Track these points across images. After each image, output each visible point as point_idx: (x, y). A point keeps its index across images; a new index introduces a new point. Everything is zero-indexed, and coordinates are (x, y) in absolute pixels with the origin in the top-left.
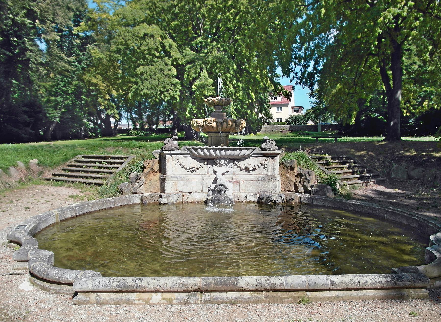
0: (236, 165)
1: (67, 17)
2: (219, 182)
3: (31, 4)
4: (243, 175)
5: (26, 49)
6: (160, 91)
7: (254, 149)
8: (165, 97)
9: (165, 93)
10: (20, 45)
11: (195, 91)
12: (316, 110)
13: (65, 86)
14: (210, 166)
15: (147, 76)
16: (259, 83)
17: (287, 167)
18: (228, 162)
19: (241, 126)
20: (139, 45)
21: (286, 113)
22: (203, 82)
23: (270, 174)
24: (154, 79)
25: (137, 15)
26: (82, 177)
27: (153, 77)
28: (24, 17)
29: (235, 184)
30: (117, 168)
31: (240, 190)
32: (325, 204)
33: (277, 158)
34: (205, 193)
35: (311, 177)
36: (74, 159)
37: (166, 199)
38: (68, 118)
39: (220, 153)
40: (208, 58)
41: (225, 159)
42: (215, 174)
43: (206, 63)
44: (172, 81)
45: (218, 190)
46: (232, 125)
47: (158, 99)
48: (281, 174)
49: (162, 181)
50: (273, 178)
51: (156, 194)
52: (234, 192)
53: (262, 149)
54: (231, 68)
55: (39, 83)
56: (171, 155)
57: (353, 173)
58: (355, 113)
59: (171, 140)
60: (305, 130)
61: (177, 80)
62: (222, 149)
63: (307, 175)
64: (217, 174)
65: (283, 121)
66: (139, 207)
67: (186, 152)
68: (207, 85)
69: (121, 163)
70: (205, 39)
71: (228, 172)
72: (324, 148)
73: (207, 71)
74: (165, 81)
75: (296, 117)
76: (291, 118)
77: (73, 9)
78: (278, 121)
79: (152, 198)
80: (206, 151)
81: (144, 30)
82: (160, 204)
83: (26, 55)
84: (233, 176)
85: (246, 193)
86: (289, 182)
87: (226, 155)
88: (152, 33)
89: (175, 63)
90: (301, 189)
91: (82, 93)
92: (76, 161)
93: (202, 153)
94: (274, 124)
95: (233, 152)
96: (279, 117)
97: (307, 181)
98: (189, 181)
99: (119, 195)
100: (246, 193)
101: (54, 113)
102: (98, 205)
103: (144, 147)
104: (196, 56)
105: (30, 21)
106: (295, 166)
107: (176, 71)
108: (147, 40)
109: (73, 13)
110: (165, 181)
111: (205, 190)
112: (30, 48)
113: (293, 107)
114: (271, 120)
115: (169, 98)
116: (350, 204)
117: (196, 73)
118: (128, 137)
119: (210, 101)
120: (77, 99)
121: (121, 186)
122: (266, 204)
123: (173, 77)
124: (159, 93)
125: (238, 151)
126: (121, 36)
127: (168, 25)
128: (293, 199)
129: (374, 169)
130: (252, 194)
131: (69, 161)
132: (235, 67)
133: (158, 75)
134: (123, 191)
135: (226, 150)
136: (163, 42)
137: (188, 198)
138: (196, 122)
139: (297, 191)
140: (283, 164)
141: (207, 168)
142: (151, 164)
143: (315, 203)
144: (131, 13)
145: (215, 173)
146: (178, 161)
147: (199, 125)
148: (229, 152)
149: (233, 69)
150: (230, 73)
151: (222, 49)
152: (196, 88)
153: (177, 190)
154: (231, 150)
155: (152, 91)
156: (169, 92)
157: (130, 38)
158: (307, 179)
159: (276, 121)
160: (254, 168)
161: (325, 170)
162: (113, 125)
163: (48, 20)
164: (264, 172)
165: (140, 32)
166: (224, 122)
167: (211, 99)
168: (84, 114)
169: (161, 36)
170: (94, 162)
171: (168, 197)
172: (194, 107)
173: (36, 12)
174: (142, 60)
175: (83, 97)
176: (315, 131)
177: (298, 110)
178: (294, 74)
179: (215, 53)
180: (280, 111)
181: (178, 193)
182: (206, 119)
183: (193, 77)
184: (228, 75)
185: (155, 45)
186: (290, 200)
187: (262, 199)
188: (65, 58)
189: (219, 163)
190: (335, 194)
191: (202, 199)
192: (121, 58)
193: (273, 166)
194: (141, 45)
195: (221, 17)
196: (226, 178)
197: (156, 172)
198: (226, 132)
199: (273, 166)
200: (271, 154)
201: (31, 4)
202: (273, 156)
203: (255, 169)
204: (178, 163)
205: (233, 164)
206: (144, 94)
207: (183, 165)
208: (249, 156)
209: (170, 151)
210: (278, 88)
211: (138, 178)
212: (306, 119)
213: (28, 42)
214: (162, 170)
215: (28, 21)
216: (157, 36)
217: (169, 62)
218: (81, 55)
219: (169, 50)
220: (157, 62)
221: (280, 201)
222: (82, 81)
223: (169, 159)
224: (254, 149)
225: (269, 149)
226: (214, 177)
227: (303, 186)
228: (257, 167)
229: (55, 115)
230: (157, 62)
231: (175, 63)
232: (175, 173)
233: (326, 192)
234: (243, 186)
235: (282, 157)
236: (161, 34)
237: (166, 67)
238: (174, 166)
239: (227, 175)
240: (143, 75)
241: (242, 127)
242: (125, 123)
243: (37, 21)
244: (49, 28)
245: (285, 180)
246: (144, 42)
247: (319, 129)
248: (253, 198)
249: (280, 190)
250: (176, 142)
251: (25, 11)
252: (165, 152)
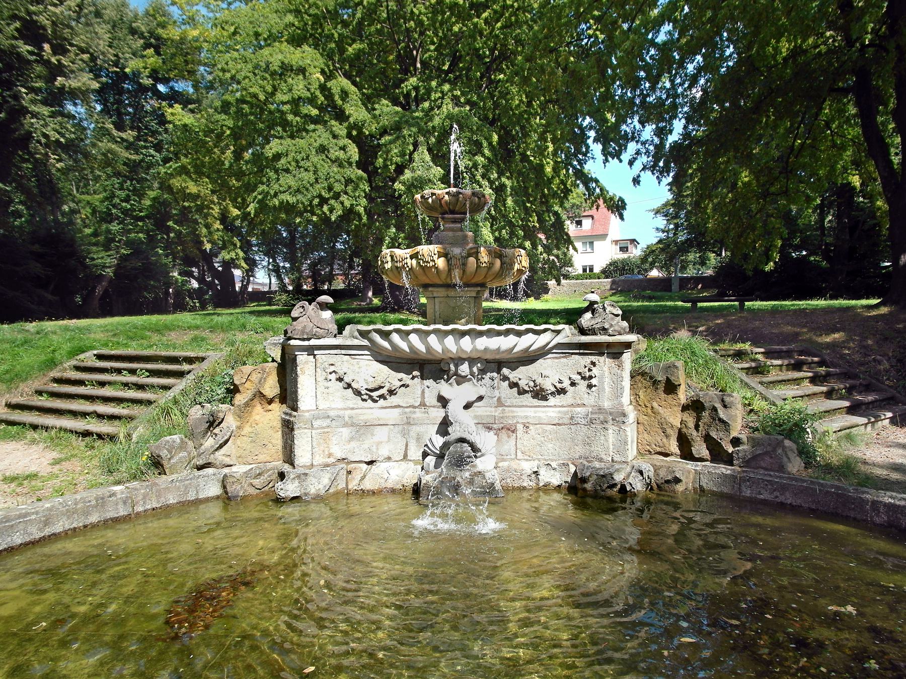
1: (130, 50)
2: (455, 432)
3: (33, 8)
5: (24, 111)
6: (320, 196)
7: (558, 332)
8: (331, 210)
9: (332, 202)
10: (8, 102)
11: (400, 196)
12: (669, 245)
13: (127, 200)
14: (430, 382)
15: (289, 163)
16: (550, 181)
17: (655, 383)
18: (483, 372)
19: (517, 267)
20: (269, 89)
21: (602, 255)
22: (419, 173)
23: (607, 404)
24: (306, 170)
25: (263, 25)
26: (74, 414)
27: (302, 163)
28: (16, 38)
30: (166, 388)
31: (519, 453)
32: (781, 499)
34: (416, 462)
35: (732, 411)
36: (74, 362)
37: (296, 483)
38: (136, 269)
39: (457, 343)
40: (431, 120)
42: (444, 407)
43: (427, 133)
44: (348, 173)
46: (491, 264)
47: (318, 215)
49: (288, 427)
51: (269, 466)
52: (501, 457)
53: (583, 331)
54: (485, 144)
55: (78, 195)
56: (311, 350)
57: (829, 395)
58: (779, 243)
59: (311, 308)
60: (644, 290)
61: (360, 172)
62: (463, 334)
63: (718, 406)
64: (450, 406)
65: (597, 270)
66: (215, 511)
67: (356, 342)
68: (430, 180)
69: (180, 374)
70: (423, 81)
71: (480, 398)
72: (729, 325)
73: (430, 150)
74: (331, 174)
75: (624, 262)
76: (613, 263)
77: (142, 33)
78: (584, 270)
79: (256, 482)
81: (280, 57)
82: (279, 501)
83: (22, 125)
84: (498, 412)
86: (663, 428)
88: (301, 63)
89: (354, 133)
90: (700, 449)
91: (169, 217)
92: (78, 368)
93: (404, 345)
94: (577, 278)
96: (588, 263)
97: (721, 426)
99: (152, 472)
100: (536, 462)
101: (102, 258)
102: (70, 513)
103: (267, 330)
104: (404, 116)
105: (29, 48)
106: (681, 378)
107: (357, 150)
108: (290, 80)
109: (142, 41)
110: (292, 430)
111: (415, 453)
112: (33, 108)
113: (616, 242)
114: (570, 269)
115: (340, 212)
116: (874, 503)
117: (402, 154)
118: (268, 308)
119: (430, 200)
120: (158, 229)
121: (157, 447)
122: (596, 495)
123: (350, 164)
124: (316, 201)
125: (512, 340)
126: (229, 71)
127: (342, 51)
128: (677, 481)
129: (878, 380)
130: (554, 464)
131: (58, 368)
132: (495, 138)
133: (315, 159)
134: (165, 463)
136: (329, 84)
138: (392, 257)
139: (687, 454)
140: (643, 374)
141: (420, 389)
142: (255, 377)
143: (747, 493)
144: (251, 19)
145: (443, 401)
146: (332, 369)
147: (399, 265)
149: (490, 144)
150: (483, 155)
151: (462, 100)
152: (403, 188)
153: (330, 455)
154: (490, 333)
155: (300, 197)
156: (341, 199)
157: (249, 74)
158: (720, 420)
159: (581, 272)
160: (559, 386)
161: (760, 388)
162: (238, 286)
163: (72, 45)
164: (590, 399)
165: (271, 60)
166: (469, 255)
167: (433, 194)
168: (174, 261)
169: (323, 72)
170: (119, 371)
171: (302, 477)
172: (402, 235)
173: (44, 28)
174: (279, 129)
175: (170, 223)
176: (666, 291)
177: (627, 248)
178: (639, 146)
179: (448, 107)
180: (589, 250)
181: (333, 464)
182: (419, 248)
183: (396, 163)
184: (480, 159)
185: (308, 90)
186: (667, 482)
187: (584, 480)
188: (115, 133)
189: (456, 374)
190: (808, 465)
191: (405, 482)
192: (230, 123)
193: (614, 379)
194: (275, 89)
195: (460, 29)
196: (476, 417)
197: (270, 402)
198: (476, 285)
199: (614, 379)
200: (609, 345)
201: (33, 8)
202: (615, 351)
203: (562, 391)
205: (495, 375)
206: (281, 203)
207: (347, 379)
208: (542, 353)
209: (309, 339)
210: (594, 189)
211: (213, 422)
212: (647, 266)
213: (27, 94)
214: (288, 395)
215: (25, 48)
216: (311, 70)
217: (340, 129)
218: (160, 134)
219: (340, 102)
220: (314, 131)
221: (638, 485)
222: (169, 189)
223: (307, 363)
224: (558, 332)
225: (604, 329)
226: (439, 414)
227: (708, 438)
228: (566, 384)
229: (105, 261)
230: (314, 131)
231: (354, 133)
233: (785, 459)
234: (525, 440)
235: (636, 352)
236: (323, 66)
237: (335, 141)
238: (322, 383)
239: (479, 409)
240: (279, 160)
241: (520, 272)
242: (262, 279)
243: (47, 47)
244: (73, 63)
245: (650, 420)
246: (284, 84)
247: (675, 286)
248: (557, 474)
249: (635, 452)
251: (18, 24)
252: (292, 342)
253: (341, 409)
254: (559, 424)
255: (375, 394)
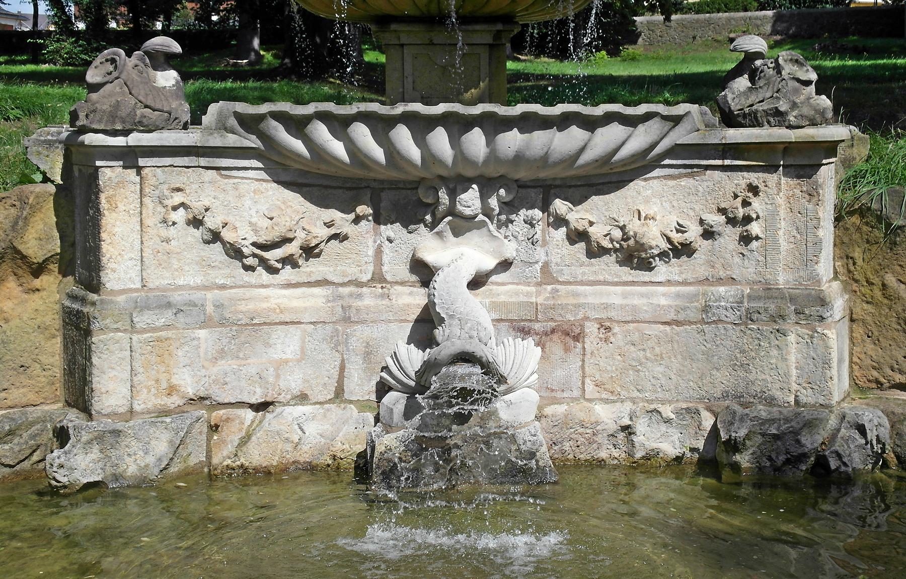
0: (560, 221)
2: (450, 339)
4: (607, 290)
7: (676, 120)
14: (393, 230)
18: (510, 207)
23: (783, 279)
29: (556, 347)
31: (590, 387)
33: (828, 174)
34: (362, 406)
39: (455, 142)
41: (487, 185)
45: (445, 393)
48: (848, 273)
49: (77, 330)
50: (809, 307)
51: (35, 413)
56: (130, 157)
59: (131, 63)
60: (845, 33)
62: (468, 123)
64: (439, 280)
67: (232, 140)
71: (505, 265)
80: (362, 133)
82: (53, 494)
85: (628, 406)
87: (493, 156)
93: (338, 148)
95: (540, 141)
98: (256, 327)
100: (628, 406)
110: (88, 333)
111: (361, 386)
125: (576, 135)
130: (668, 411)
135: (494, 125)
137: (245, 441)
140: (863, 212)
141: (372, 245)
145: (424, 272)
146: (178, 198)
148: (512, 141)
153: (172, 390)
154: (527, 123)
160: (677, 237)
164: (746, 269)
181: (179, 411)
189: (452, 211)
191: (338, 447)
197: (38, 270)
200: (788, 148)
202: (802, 161)
203: (684, 250)
204: (180, 216)
205: (537, 213)
207: (212, 222)
208: (641, 165)
209: (126, 133)
214: (80, 256)
223: (121, 184)
224: (676, 120)
225: (777, 113)
226: (413, 299)
232: (158, 279)
234: (603, 358)
238: (155, 230)
239: (503, 289)
250: (168, 78)
252: (90, 139)
253: (198, 288)
254: (678, 323)
255: (272, 256)
